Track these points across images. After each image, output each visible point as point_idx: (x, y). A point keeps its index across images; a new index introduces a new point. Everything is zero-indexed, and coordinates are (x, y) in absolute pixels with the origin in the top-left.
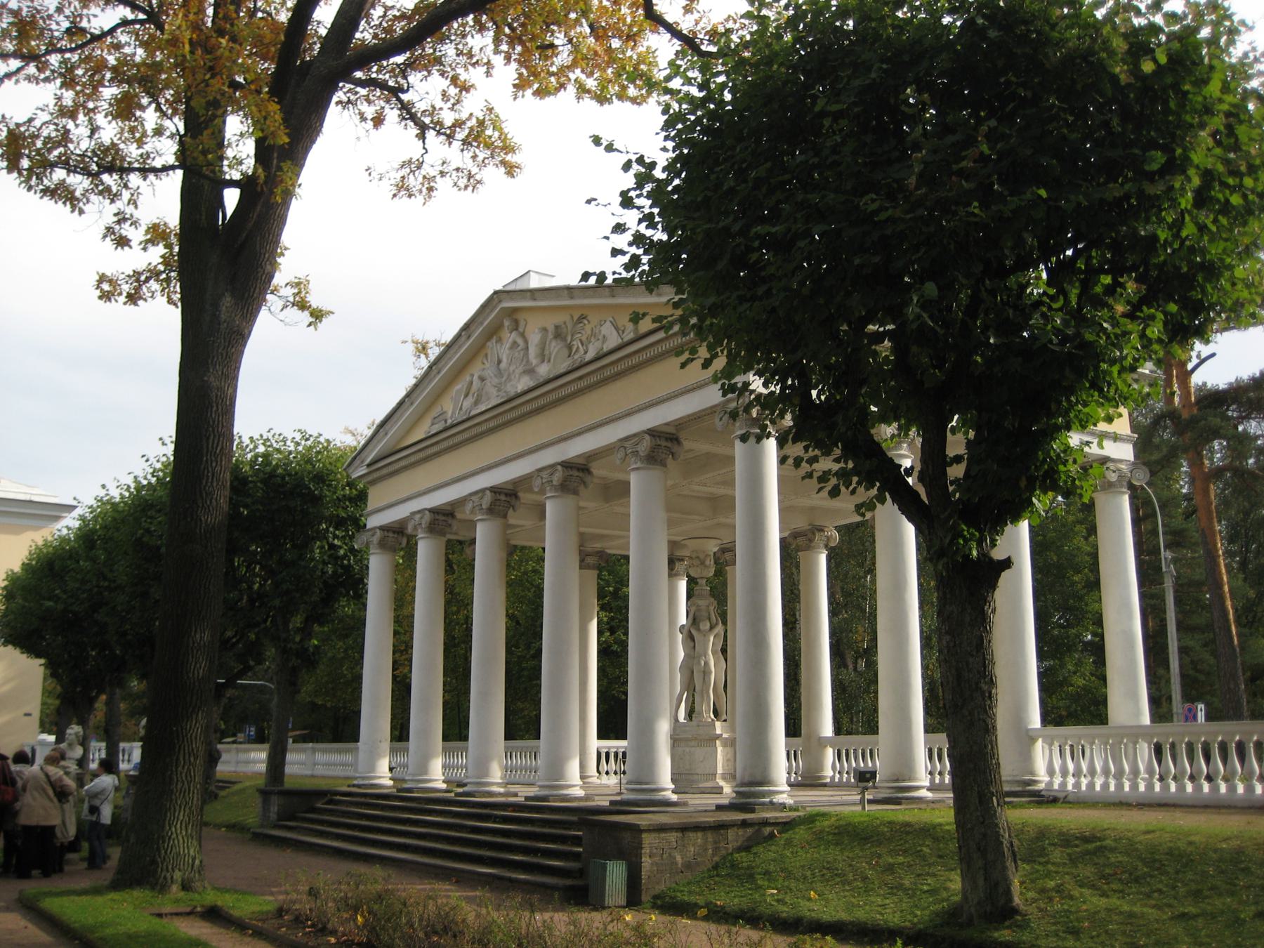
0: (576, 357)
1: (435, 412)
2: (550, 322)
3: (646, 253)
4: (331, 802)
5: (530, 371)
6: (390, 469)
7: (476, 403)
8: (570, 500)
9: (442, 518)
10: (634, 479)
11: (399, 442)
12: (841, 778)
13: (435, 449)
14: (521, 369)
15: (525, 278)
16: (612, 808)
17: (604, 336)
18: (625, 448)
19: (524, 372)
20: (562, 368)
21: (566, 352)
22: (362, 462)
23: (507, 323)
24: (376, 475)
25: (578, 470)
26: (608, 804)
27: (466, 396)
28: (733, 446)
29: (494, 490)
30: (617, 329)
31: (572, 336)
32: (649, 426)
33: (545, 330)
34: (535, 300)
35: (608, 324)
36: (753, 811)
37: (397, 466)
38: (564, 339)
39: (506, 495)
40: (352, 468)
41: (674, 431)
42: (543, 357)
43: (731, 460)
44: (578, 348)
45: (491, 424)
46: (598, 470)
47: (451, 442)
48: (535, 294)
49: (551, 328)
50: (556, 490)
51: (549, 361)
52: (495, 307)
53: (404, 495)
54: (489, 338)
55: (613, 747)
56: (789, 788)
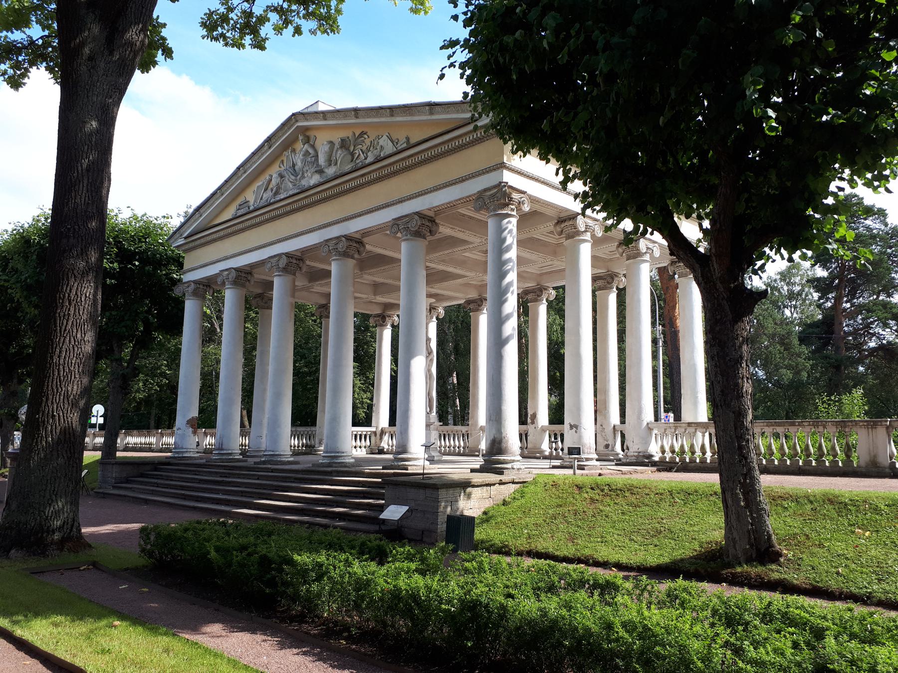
0: (357, 162)
1: (240, 200)
2: (336, 137)
3: (516, 40)
4: (156, 470)
5: (320, 172)
6: (203, 241)
7: (276, 193)
8: (290, 278)
9: (242, 276)
10: (334, 268)
11: (209, 223)
12: (445, 450)
13: (241, 226)
14: (313, 170)
15: (315, 105)
16: (314, 469)
17: (382, 146)
18: (398, 225)
19: (316, 172)
20: (348, 167)
21: (349, 157)
22: (181, 235)
23: (301, 138)
24: (191, 245)
25: (356, 242)
26: (311, 465)
27: (266, 190)
28: (330, 264)
29: (288, 255)
30: (392, 141)
31: (354, 146)
32: (417, 210)
33: (331, 143)
34: (325, 119)
35: (385, 137)
36: (407, 469)
37: (209, 238)
38: (348, 149)
39: (204, 285)
40: (173, 240)
41: (433, 216)
42: (330, 162)
43: (328, 274)
44: (359, 154)
45: (288, 208)
46: (258, 276)
47: (253, 221)
48: (325, 114)
49: (337, 142)
50: (232, 284)
51: (336, 164)
52: (292, 125)
53: (215, 259)
54: (285, 149)
55: (364, 431)
56: (521, 458)
